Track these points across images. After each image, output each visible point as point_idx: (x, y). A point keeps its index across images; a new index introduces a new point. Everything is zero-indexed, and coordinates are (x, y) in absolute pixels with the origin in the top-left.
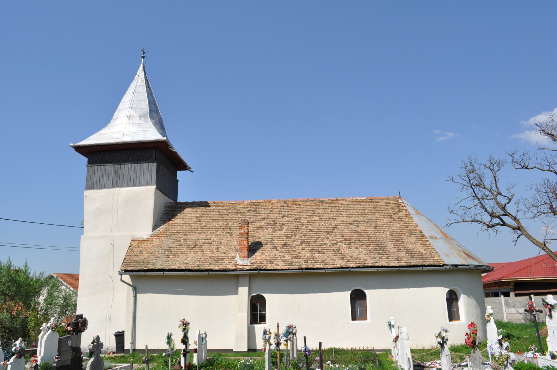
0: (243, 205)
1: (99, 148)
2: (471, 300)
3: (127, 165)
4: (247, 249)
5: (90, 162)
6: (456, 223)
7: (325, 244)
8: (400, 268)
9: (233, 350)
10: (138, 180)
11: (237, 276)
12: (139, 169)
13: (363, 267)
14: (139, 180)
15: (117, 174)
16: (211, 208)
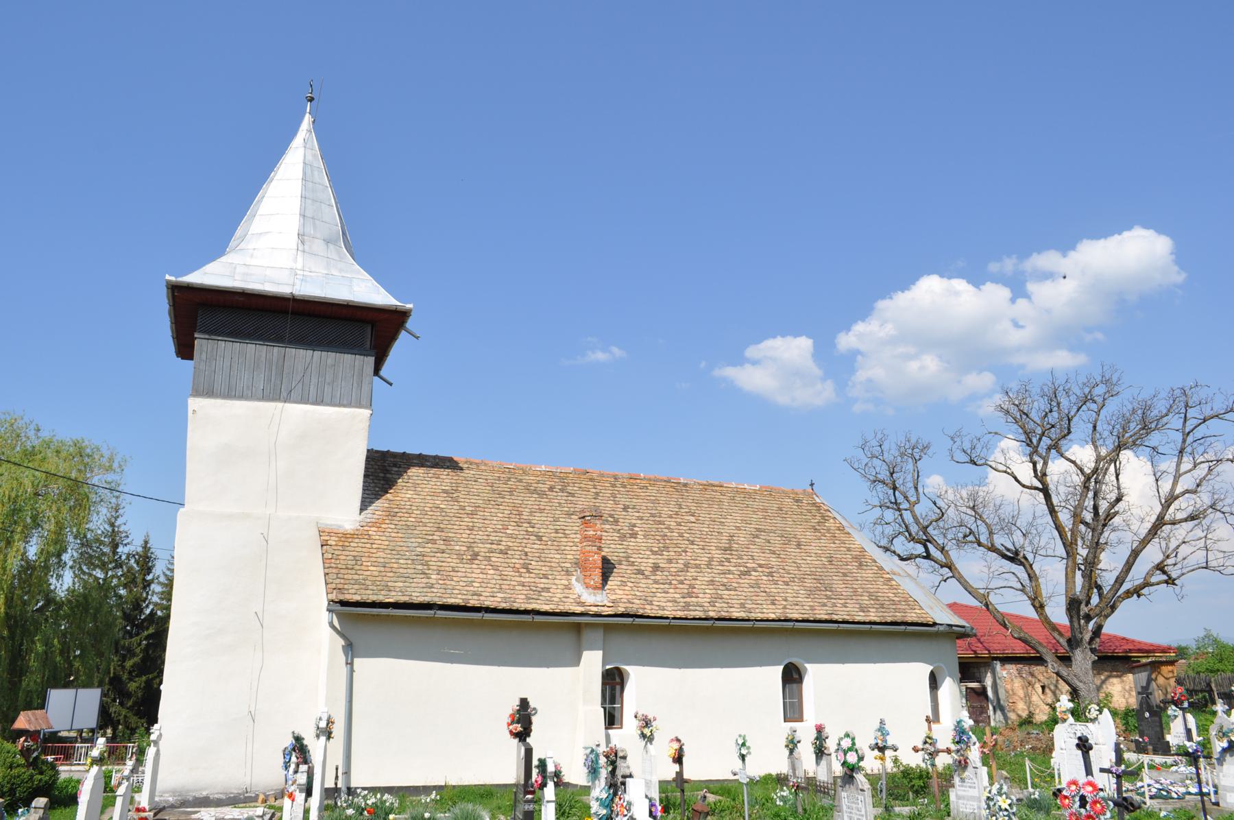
0: (533, 475)
1: (241, 299)
3: (302, 352)
4: (601, 571)
7: (730, 572)
8: (873, 626)
10: (327, 389)
11: (578, 628)
12: (332, 366)
14: (330, 390)
16: (468, 473)
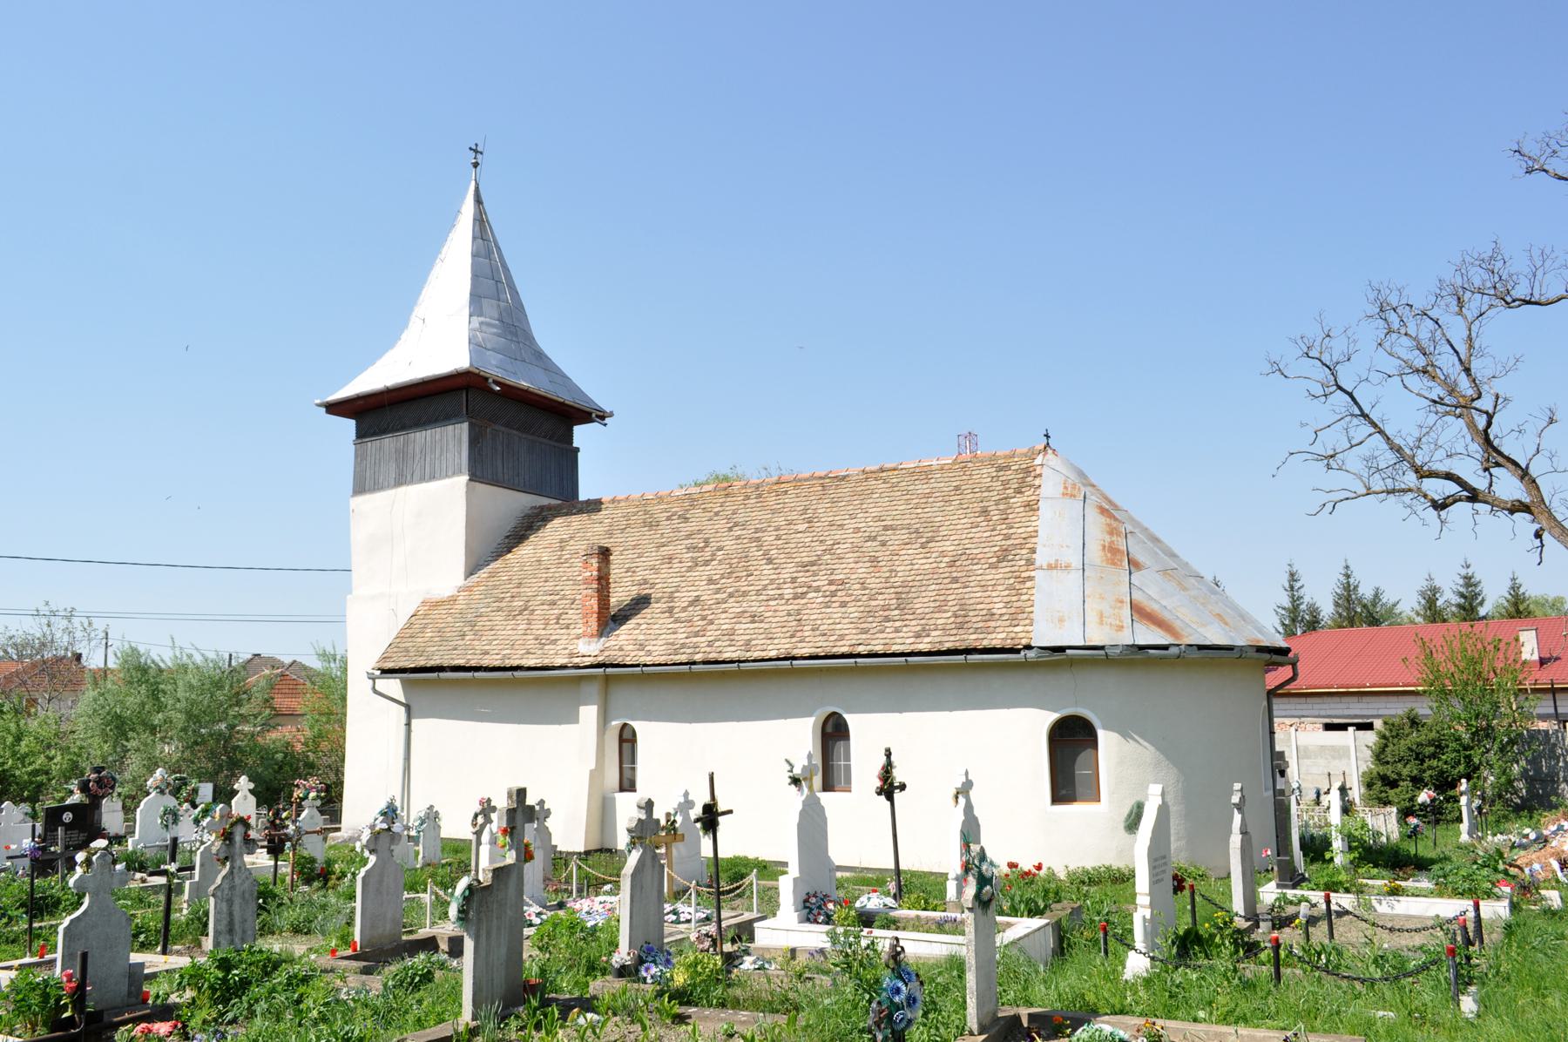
2: (1137, 745)
5: (361, 434)
6: (1347, 499)
13: (885, 655)
15: (402, 456)
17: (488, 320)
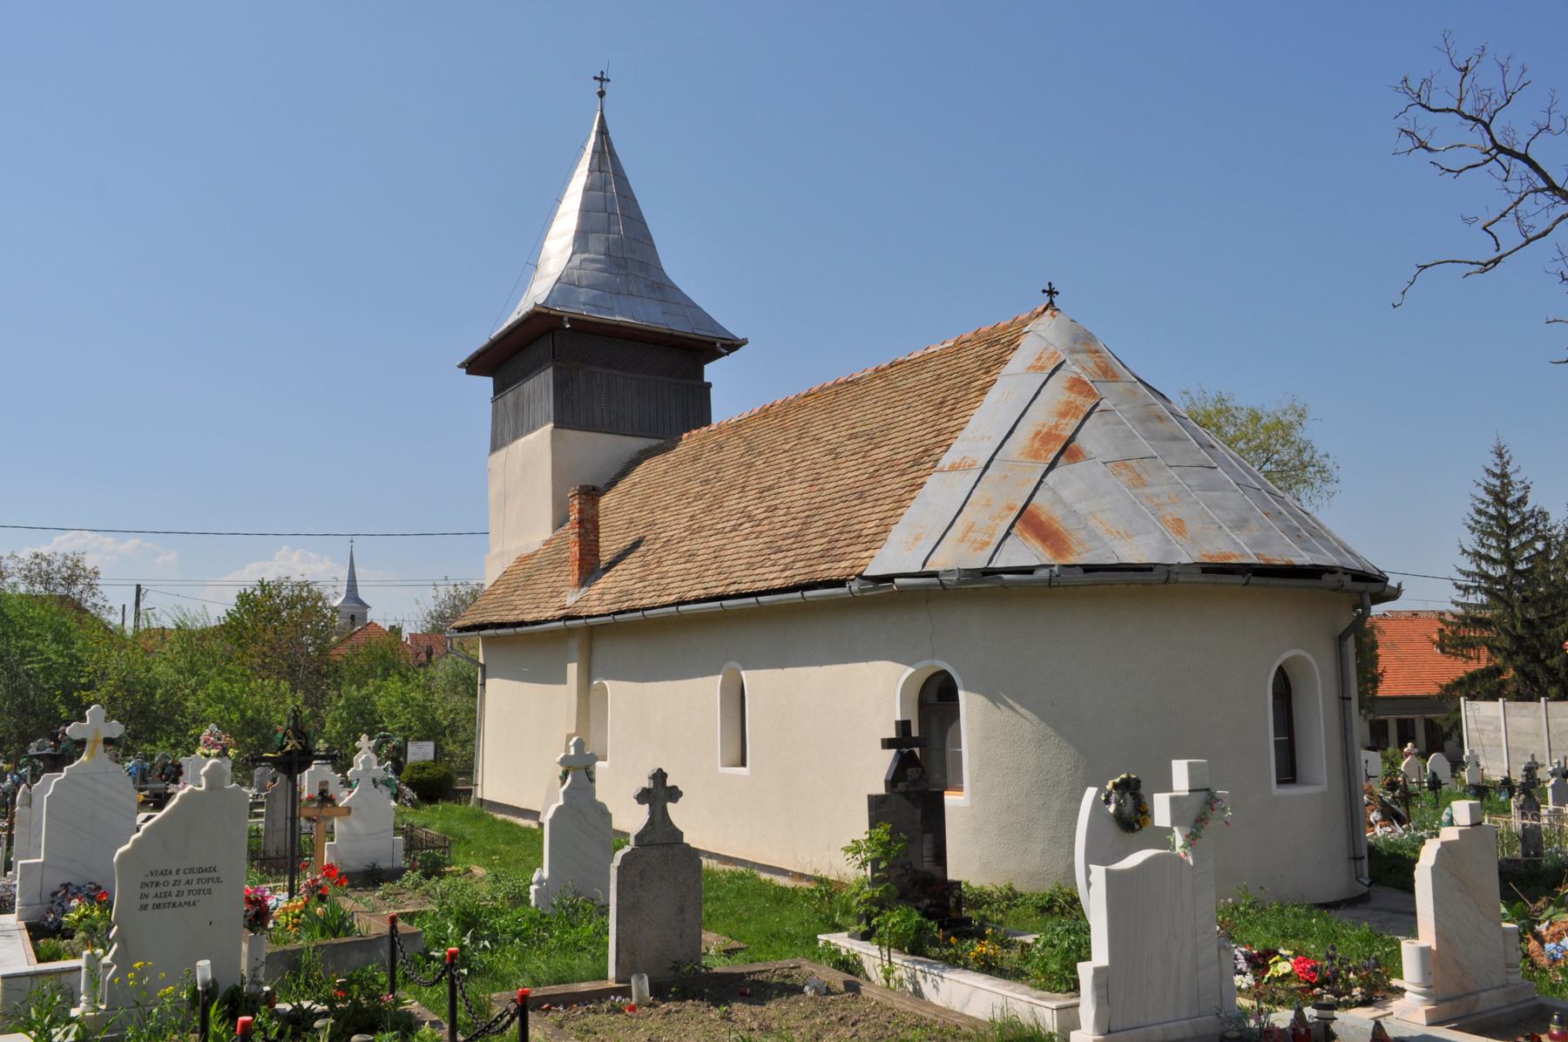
2: (1011, 713)
9: (1079, 1027)
17: (593, 256)
